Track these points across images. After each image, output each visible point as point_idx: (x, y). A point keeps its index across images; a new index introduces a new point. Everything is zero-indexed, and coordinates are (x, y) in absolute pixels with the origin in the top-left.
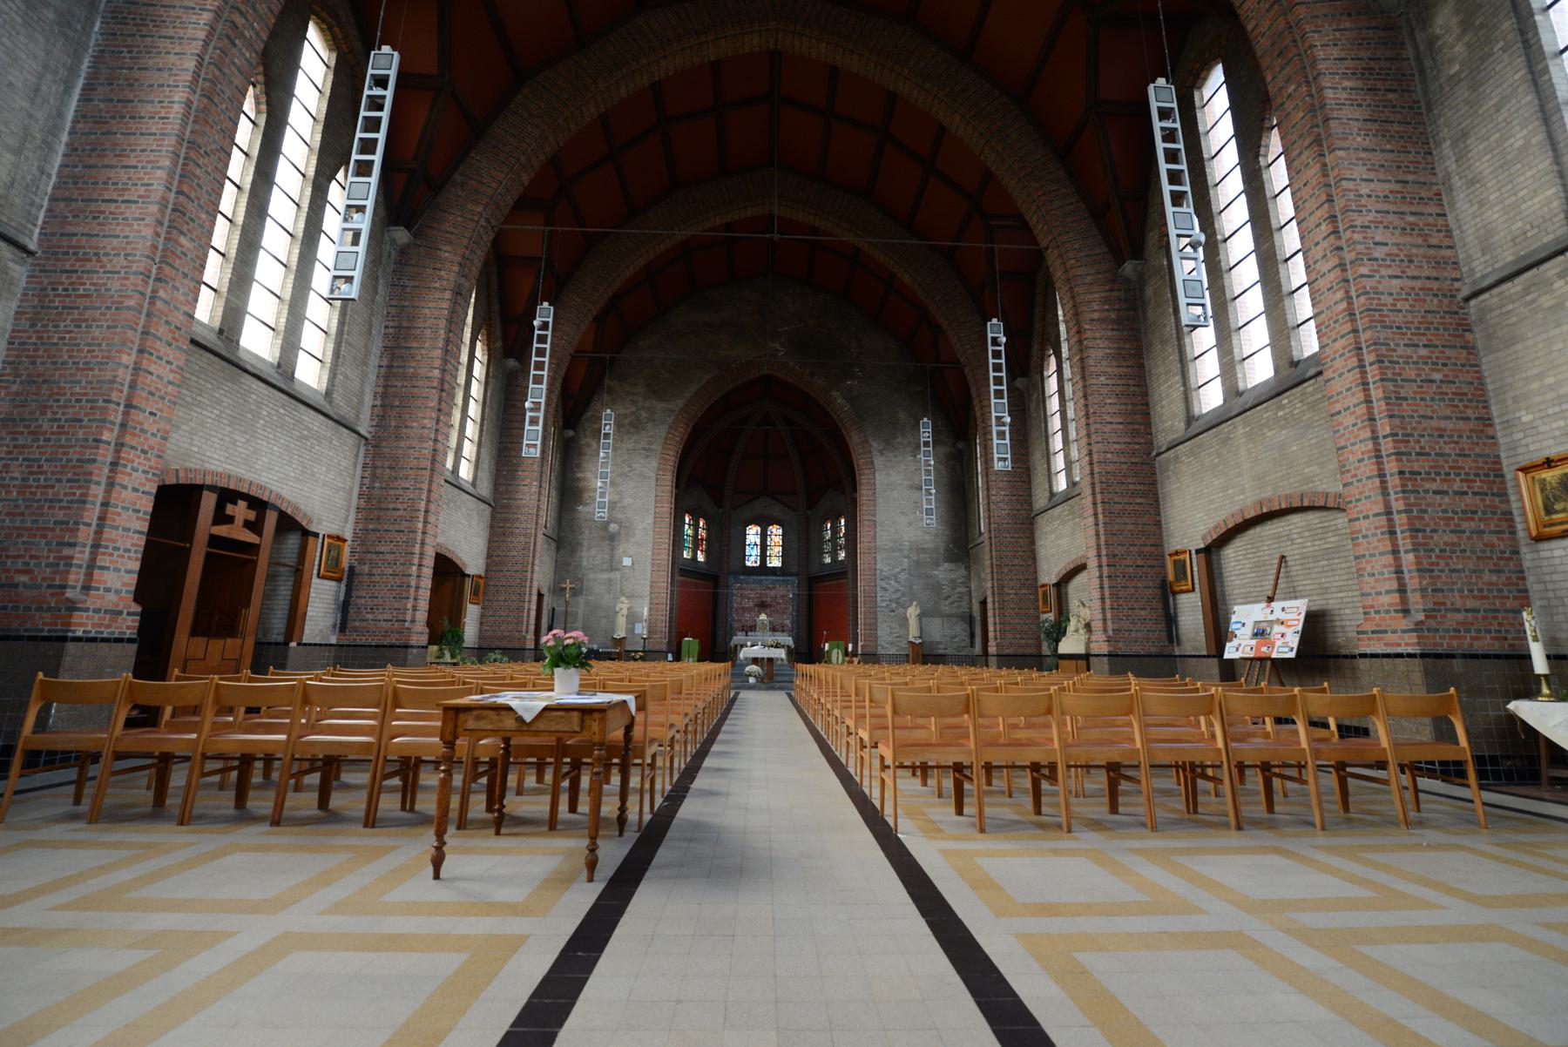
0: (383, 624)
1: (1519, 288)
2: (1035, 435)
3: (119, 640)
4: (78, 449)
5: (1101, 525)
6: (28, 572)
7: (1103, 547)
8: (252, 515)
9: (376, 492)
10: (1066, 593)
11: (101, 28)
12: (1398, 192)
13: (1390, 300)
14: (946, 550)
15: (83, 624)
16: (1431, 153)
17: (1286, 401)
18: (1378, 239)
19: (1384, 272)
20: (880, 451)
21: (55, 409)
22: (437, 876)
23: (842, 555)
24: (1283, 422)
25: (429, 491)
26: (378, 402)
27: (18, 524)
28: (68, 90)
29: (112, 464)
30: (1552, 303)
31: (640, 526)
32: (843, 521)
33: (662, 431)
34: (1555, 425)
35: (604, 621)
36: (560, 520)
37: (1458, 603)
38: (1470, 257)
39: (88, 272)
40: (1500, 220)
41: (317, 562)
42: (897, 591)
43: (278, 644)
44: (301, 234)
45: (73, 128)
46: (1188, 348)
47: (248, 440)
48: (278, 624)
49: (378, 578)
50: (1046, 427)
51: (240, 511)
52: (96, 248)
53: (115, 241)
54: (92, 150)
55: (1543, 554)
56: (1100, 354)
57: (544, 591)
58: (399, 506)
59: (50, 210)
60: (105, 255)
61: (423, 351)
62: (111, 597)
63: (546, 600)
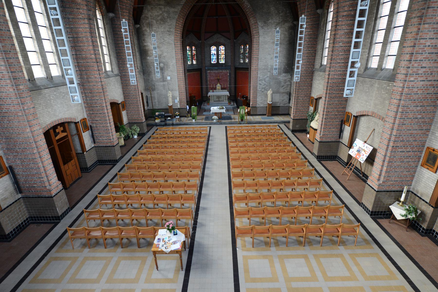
0: (105, 141)
2: (320, 37)
3: (61, 191)
5: (327, 101)
6: (35, 184)
7: (326, 109)
8: (62, 129)
9: (88, 101)
10: (319, 102)
14: (284, 68)
15: (54, 193)
17: (391, 85)
20: (262, 27)
22: (158, 270)
23: (247, 61)
24: (387, 91)
25: (105, 99)
27: (26, 174)
32: (248, 46)
33: (174, 22)
35: (164, 99)
41: (81, 129)
42: (265, 84)
43: (81, 153)
46: (375, 38)
47: (52, 109)
48: (79, 150)
49: (99, 128)
50: (325, 36)
53: (4, 94)
55: (422, 170)
57: (143, 92)
58: (97, 106)
60: (4, 98)
61: (86, 47)
62: (55, 184)
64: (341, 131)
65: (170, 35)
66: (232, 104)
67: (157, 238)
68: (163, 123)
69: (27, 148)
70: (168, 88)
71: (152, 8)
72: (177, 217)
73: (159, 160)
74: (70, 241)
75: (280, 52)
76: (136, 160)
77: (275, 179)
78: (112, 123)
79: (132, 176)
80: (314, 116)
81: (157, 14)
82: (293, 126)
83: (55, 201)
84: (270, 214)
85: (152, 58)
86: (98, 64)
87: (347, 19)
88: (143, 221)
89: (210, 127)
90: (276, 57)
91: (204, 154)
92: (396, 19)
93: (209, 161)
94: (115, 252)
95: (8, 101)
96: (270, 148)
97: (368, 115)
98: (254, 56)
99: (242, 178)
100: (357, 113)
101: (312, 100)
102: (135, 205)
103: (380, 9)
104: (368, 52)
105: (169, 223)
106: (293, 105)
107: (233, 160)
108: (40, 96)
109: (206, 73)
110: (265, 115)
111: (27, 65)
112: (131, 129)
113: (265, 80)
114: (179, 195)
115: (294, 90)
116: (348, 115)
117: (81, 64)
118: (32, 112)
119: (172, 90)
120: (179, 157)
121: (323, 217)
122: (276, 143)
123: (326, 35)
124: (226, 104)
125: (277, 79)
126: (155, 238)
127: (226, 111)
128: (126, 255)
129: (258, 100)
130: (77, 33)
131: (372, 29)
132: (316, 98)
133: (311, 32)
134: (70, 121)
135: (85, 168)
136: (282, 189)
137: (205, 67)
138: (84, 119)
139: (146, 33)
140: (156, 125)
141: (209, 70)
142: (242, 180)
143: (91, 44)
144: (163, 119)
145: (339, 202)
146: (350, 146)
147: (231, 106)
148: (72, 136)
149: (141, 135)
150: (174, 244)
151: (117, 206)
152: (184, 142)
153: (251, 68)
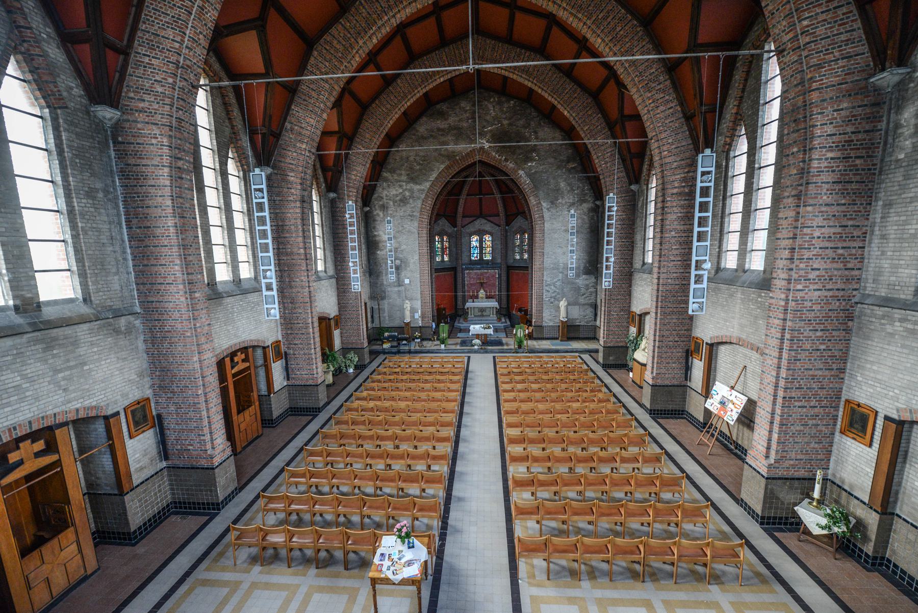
1: (881, 313)
6: (192, 445)
7: (658, 331)
11: (120, 183)
12: (839, 233)
13: (810, 304)
16: (870, 204)
17: (763, 295)
18: (815, 266)
19: (812, 287)
20: (548, 209)
25: (312, 313)
26: (277, 269)
28: (121, 227)
30: (892, 331)
31: (412, 261)
34: (869, 390)
36: (369, 260)
37: (793, 456)
38: (867, 279)
40: (887, 270)
42: (555, 292)
44: (223, 207)
45: (130, 244)
50: (646, 221)
51: (240, 357)
54: (143, 256)
57: (367, 301)
59: (138, 290)
61: (293, 239)
62: (221, 446)
64: (688, 368)
65: (412, 220)
66: (503, 320)
67: (379, 552)
71: (389, 186)
72: (413, 514)
73: (386, 410)
75: (577, 243)
76: (349, 410)
77: (580, 449)
78: (318, 349)
81: (395, 192)
84: (576, 514)
88: (356, 519)
89: (469, 357)
90: (572, 252)
93: (468, 414)
95: (176, 315)
96: (569, 394)
97: (731, 343)
99: (524, 446)
102: (344, 489)
105: (402, 524)
106: (602, 324)
107: (508, 413)
109: (463, 274)
110: (557, 339)
111: (209, 263)
112: (345, 358)
113: (554, 284)
114: (418, 473)
115: (603, 301)
118: (205, 332)
119: (411, 299)
120: (419, 405)
122: (578, 386)
126: (375, 553)
128: (323, 582)
129: (544, 315)
130: (283, 220)
132: (638, 313)
135: (269, 420)
136: (594, 468)
137: (462, 265)
139: (378, 218)
140: (384, 352)
141: (467, 269)
144: (395, 344)
146: (707, 392)
148: (256, 367)
149: (360, 368)
150: (408, 566)
152: (426, 381)
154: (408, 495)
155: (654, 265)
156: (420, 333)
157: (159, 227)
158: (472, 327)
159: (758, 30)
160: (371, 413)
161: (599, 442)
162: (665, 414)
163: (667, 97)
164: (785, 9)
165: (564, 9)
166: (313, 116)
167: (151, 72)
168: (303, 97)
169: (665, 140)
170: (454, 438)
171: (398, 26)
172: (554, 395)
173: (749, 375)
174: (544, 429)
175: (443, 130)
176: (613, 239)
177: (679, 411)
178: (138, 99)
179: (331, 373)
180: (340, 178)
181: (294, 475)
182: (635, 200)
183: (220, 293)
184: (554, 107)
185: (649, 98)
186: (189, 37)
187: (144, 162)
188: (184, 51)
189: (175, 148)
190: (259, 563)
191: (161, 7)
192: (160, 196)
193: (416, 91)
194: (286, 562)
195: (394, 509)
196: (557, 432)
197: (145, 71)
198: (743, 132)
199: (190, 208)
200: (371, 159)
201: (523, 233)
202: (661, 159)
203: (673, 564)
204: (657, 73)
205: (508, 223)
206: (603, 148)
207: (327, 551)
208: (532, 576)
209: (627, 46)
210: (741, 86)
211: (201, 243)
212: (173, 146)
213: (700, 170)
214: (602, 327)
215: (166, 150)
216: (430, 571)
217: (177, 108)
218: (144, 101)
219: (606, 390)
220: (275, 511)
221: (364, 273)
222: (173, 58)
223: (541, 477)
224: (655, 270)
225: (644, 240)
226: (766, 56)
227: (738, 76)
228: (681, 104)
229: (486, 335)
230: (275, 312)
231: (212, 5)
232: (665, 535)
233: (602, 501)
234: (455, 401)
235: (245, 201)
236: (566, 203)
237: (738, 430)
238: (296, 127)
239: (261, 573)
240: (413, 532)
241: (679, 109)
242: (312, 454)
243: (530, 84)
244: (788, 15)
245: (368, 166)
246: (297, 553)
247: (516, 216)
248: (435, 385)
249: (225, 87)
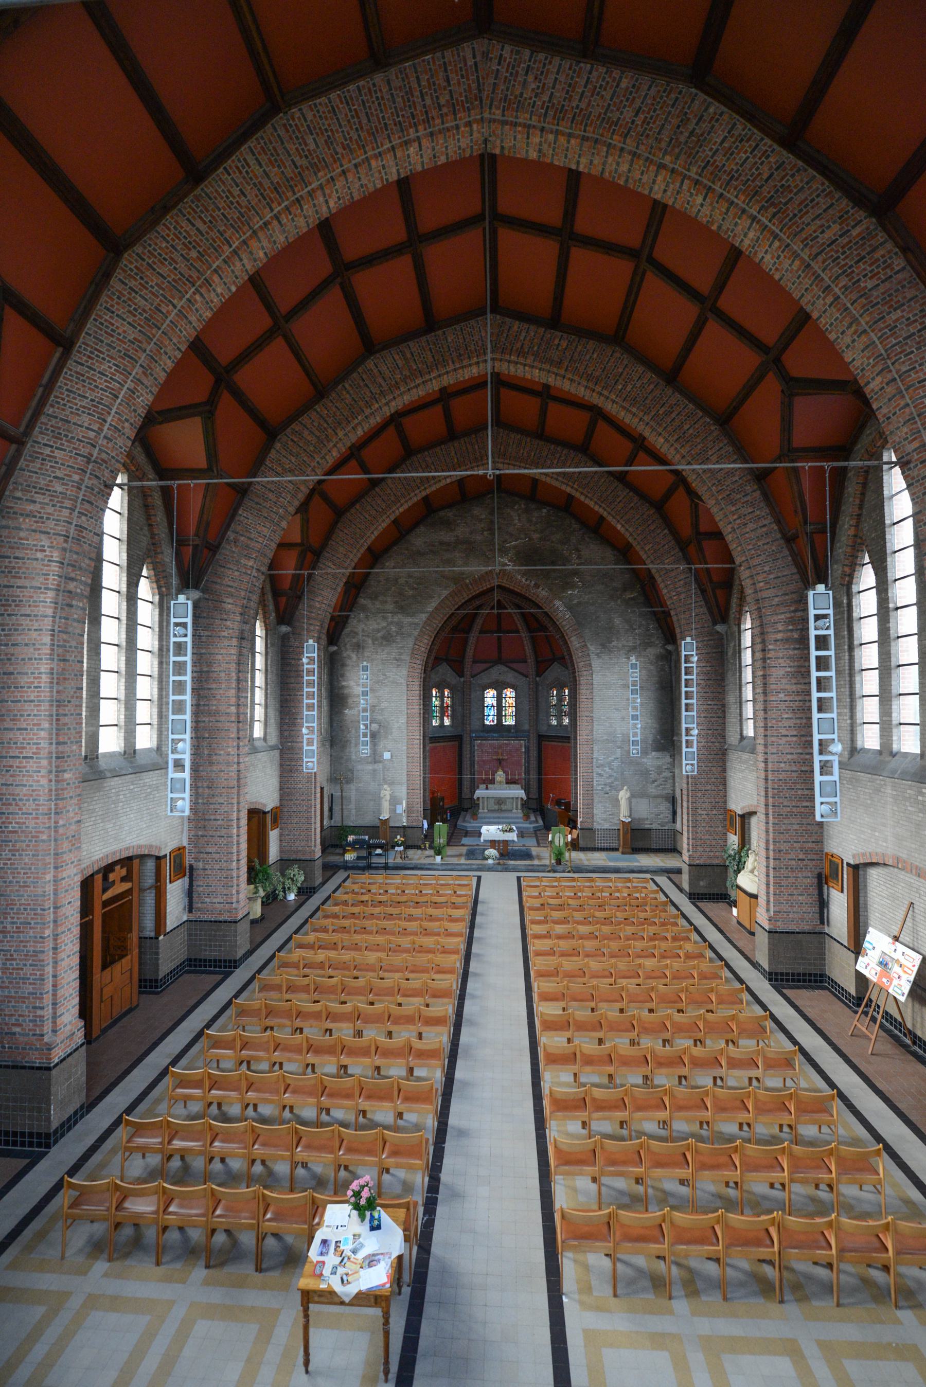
0: (218, 905)
2: (730, 678)
4: (32, 944)
5: (771, 825)
6: (20, 1025)
7: (771, 842)
9: (200, 807)
14: (654, 741)
20: (597, 655)
21: (12, 915)
22: (307, 1372)
24: (921, 806)
25: (238, 803)
27: (6, 994)
29: (53, 948)
31: (396, 725)
32: (567, 691)
35: (372, 803)
39: (12, 813)
42: (611, 776)
43: (151, 938)
44: (124, 644)
46: (858, 686)
48: (149, 923)
49: (209, 872)
52: (13, 795)
53: (25, 789)
56: (781, 672)
57: (325, 785)
58: (218, 817)
60: (20, 800)
61: (221, 692)
62: (69, 1027)
63: (325, 789)
64: (823, 904)
65: (398, 666)
66: (533, 818)
67: (319, 1236)
68: (363, 863)
69: (32, 922)
70: (384, 779)
71: (367, 617)
72: (381, 1160)
73: (344, 966)
74: (60, 1223)
75: (642, 704)
76: (285, 965)
77: (660, 1042)
78: (244, 862)
79: (270, 1012)
80: (743, 860)
81: (376, 626)
82: (690, 884)
83: (53, 1081)
84: (659, 1165)
85: (356, 713)
86: (241, 724)
87: (787, 646)
88: (282, 1168)
89: (479, 878)
90: (635, 717)
91: (463, 952)
92: (897, 651)
93: (476, 975)
94: (184, 1283)
95: (30, 806)
96: (639, 945)
97: (885, 864)
98: (583, 713)
99: (568, 1034)
100: (854, 856)
101: (731, 817)
102: (266, 1110)
103: (855, 629)
104: (848, 714)
105: (362, 1181)
106: (685, 828)
107: (542, 976)
108: (98, 794)
109: (472, 746)
110: (616, 850)
111: (92, 725)
112: (283, 875)
113: (609, 764)
114: (393, 1083)
115: (685, 792)
116: (831, 861)
117: (203, 724)
118: (70, 833)
119: (391, 784)
120: (398, 959)
121: (823, 1186)
122: (652, 930)
123: (743, 675)
124: (517, 818)
125: (638, 764)
126: (311, 1238)
127: (518, 836)
128: (216, 1296)
129: (595, 812)
130: (210, 664)
131: (847, 668)
132: (740, 812)
133: (708, 669)
134: (146, 853)
135: (151, 981)
136: (685, 1077)
137: (471, 731)
138: (179, 849)
139: (348, 662)
140: (346, 867)
141: (478, 738)
142: (569, 1041)
143: (234, 685)
144: (364, 853)
145: (822, 1084)
146: (857, 947)
147: (531, 823)
148: (142, 890)
149: (306, 892)
150: (370, 1266)
151: (214, 1109)
152: (411, 918)
153: (576, 737)
154: (374, 1125)
155: (758, 741)
156: (404, 836)
157: (27, 674)
158: (484, 829)
159: (870, 434)
160: (320, 972)
161: (689, 1029)
162: (793, 981)
163: (758, 513)
164: (903, 413)
165: (613, 401)
166: (268, 524)
167: (51, 466)
168: (256, 500)
169: (759, 568)
170: (453, 1018)
171: (392, 415)
172: (614, 945)
173: (919, 918)
174: (601, 1005)
175: (448, 544)
176: (694, 677)
177: (816, 975)
178: (27, 500)
179: (259, 901)
180: (297, 605)
181: (183, 1082)
182: (722, 645)
183: (101, 772)
184: (602, 518)
185: (733, 513)
186: (111, 425)
187: (20, 582)
188: (100, 442)
189: (68, 565)
190: (105, 1256)
191: (78, 389)
192: (36, 630)
193: (412, 494)
194: (154, 1254)
195: (350, 1150)
196: (622, 1011)
197: (42, 464)
198: (867, 559)
199: (76, 647)
200: (344, 580)
201: (561, 689)
202: (756, 592)
203: (830, 1266)
204: (741, 481)
205: (539, 673)
206: (673, 574)
207: (227, 1231)
208: (585, 1288)
209: (699, 447)
210: (857, 502)
211: (84, 696)
212: (66, 562)
213: (812, 612)
214: (685, 833)
215: (55, 567)
216: (407, 1277)
217: (79, 513)
218: (35, 502)
219: (698, 938)
220: (144, 1151)
221: (322, 743)
222: (84, 451)
223: (597, 1093)
224: (760, 749)
225: (740, 703)
226: (885, 467)
227: (852, 489)
228: (778, 522)
229: (506, 842)
230: (184, 804)
231: (147, 387)
232: (811, 1208)
233: (701, 1139)
234: (456, 952)
235: (157, 637)
236: (623, 646)
237: (913, 1011)
238: (242, 538)
239: (106, 1275)
240: (379, 1196)
241: (776, 528)
242: (217, 1043)
243: (568, 490)
244: (909, 420)
245: (339, 590)
246: (174, 1236)
247: (553, 661)
248: (426, 924)
249: (149, 488)
